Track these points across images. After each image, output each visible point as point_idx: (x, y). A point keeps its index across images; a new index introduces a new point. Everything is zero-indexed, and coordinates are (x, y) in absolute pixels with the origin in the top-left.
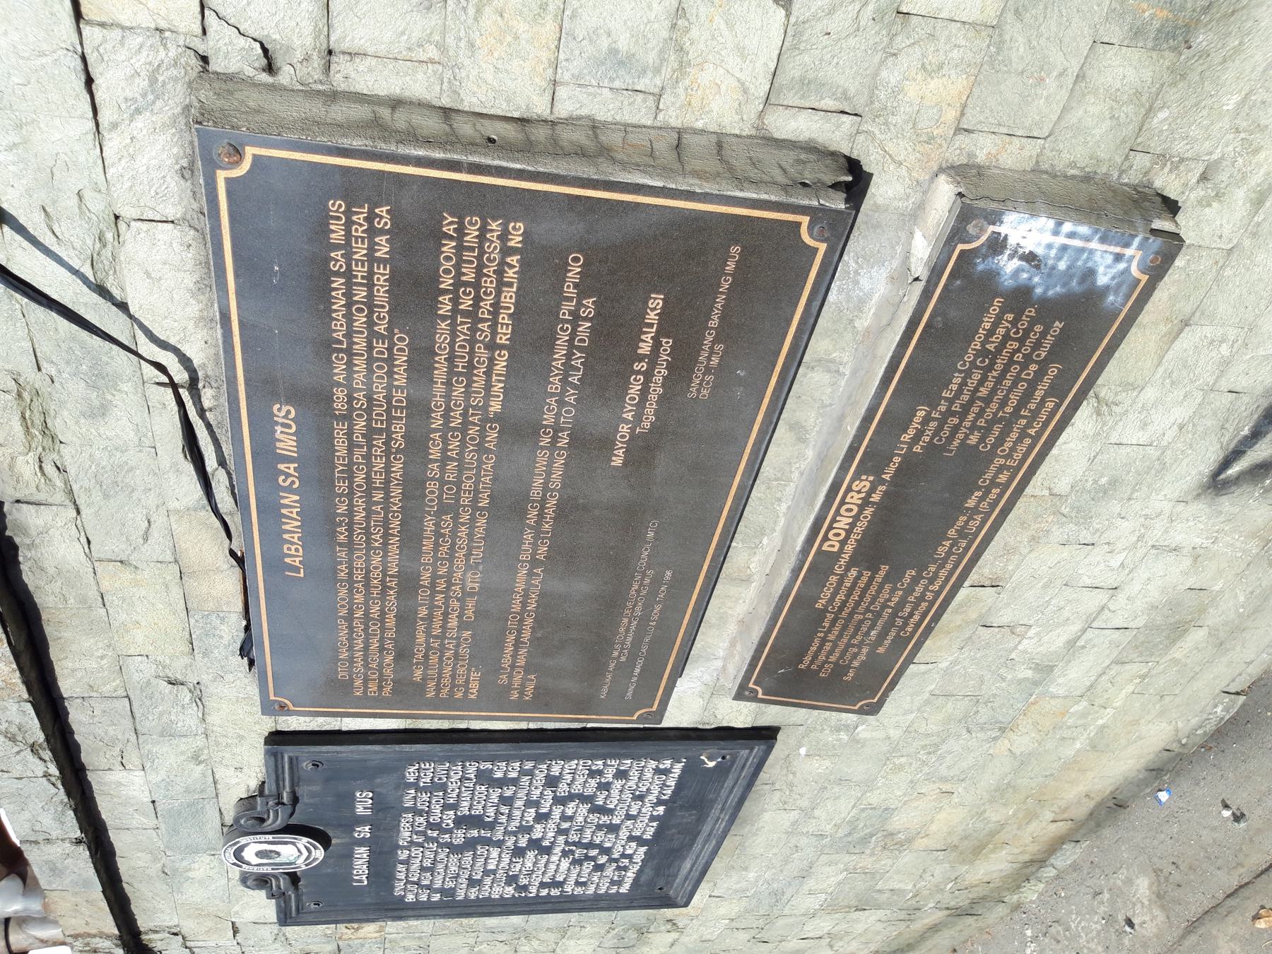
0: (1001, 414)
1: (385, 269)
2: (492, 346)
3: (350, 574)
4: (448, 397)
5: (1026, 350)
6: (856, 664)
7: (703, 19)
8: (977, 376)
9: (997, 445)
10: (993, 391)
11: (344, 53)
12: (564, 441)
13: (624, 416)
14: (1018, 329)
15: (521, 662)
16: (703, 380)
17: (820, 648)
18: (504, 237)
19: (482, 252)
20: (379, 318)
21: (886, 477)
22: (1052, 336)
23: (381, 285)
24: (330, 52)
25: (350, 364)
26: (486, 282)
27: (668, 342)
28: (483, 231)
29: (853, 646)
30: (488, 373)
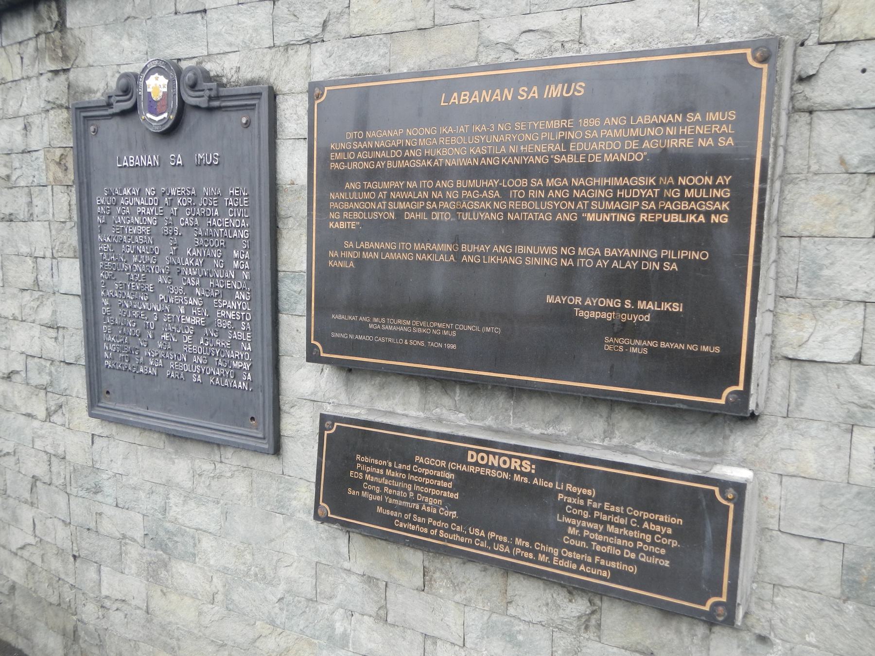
0: (594, 544)
1: (690, 144)
2: (638, 211)
3: (444, 135)
4: (597, 187)
5: (646, 548)
6: (364, 494)
7: (844, 315)
8: (622, 521)
9: (572, 548)
10: (612, 535)
11: (811, 119)
12: (564, 263)
13: (588, 299)
14: (661, 539)
15: (366, 255)
16: (619, 345)
17: (377, 466)
18: (717, 212)
19: (706, 200)
20: (375, 184)
21: (535, 481)
22: (658, 562)
23: (678, 143)
24: (811, 112)
25: (618, 127)
26: (685, 204)
27: (647, 318)
28: (721, 200)
29: (382, 489)
30: (617, 210)
